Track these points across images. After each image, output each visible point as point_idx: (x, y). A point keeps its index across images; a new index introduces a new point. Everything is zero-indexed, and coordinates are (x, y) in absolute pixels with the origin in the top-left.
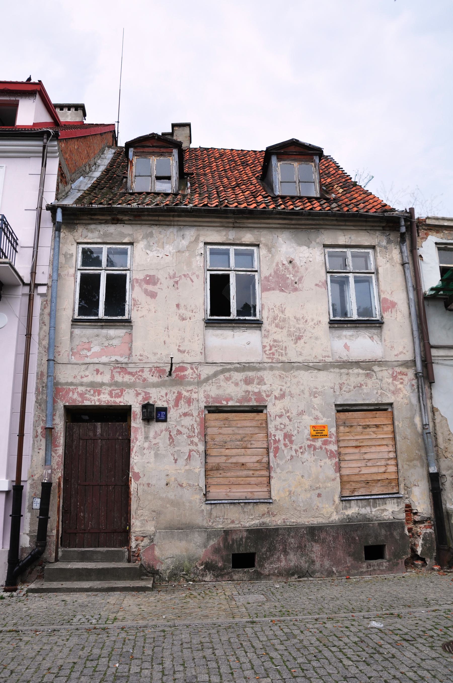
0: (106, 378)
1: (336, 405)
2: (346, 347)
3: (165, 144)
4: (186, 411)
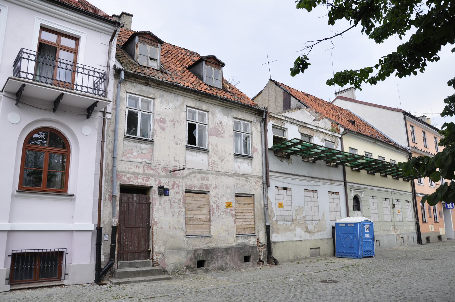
0: (141, 171)
1: (235, 193)
2: (239, 167)
3: (154, 40)
4: (177, 191)
